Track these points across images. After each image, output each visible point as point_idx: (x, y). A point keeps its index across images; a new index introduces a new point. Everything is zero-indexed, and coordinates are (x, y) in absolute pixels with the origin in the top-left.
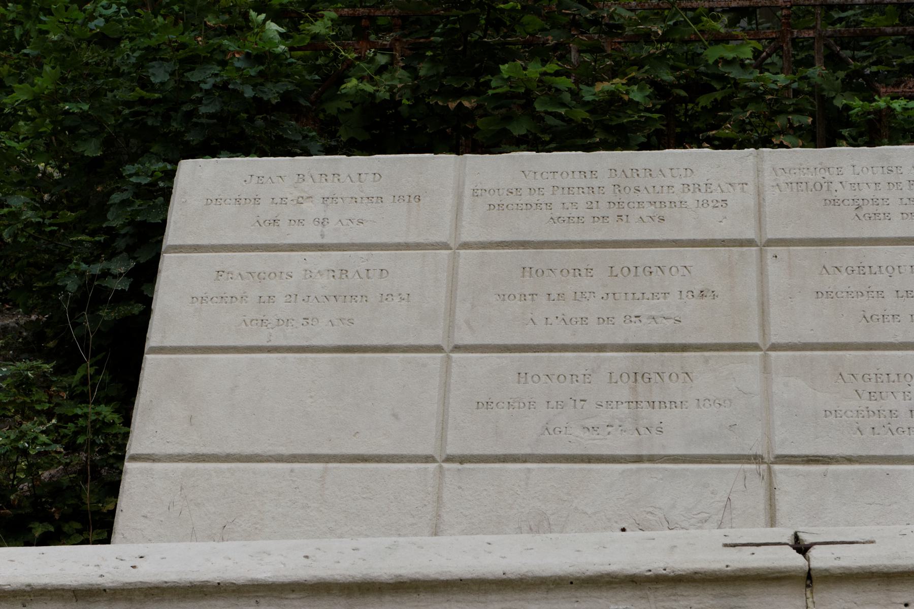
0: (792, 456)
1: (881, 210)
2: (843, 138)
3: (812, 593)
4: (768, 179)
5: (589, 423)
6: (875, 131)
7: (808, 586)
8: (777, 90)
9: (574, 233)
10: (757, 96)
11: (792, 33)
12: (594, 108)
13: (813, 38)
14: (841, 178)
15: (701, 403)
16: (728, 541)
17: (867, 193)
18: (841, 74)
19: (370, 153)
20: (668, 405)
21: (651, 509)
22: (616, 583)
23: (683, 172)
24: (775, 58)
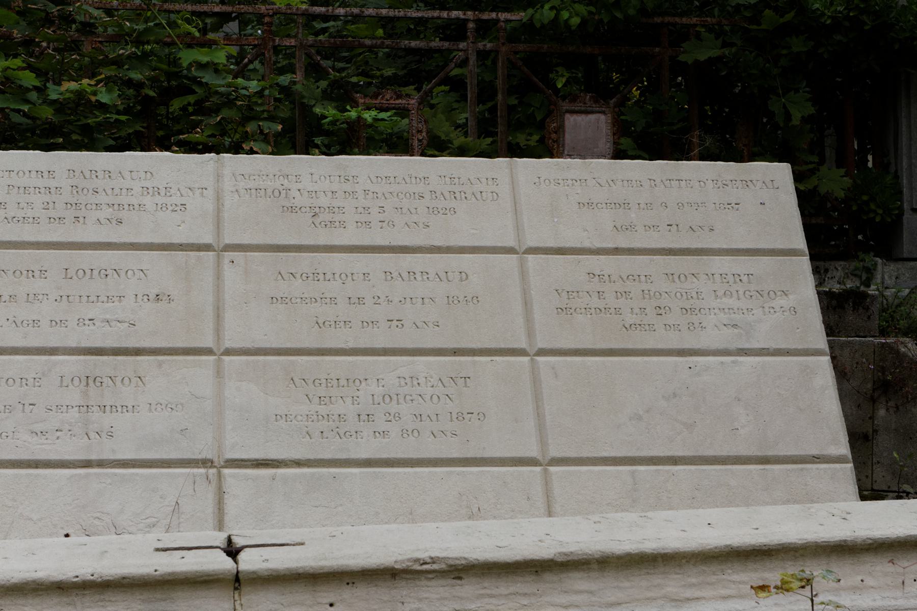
0: (242, 460)
1: (337, 218)
2: (317, 146)
3: (240, 595)
4: (228, 184)
5: (38, 427)
6: (348, 140)
7: (236, 589)
8: (249, 96)
9: (28, 234)
10: (229, 102)
11: (274, 41)
12: (59, 106)
13: (295, 47)
14: (300, 186)
15: (153, 407)
16: (160, 545)
17: (324, 201)
18: (323, 84)
19: (540, 157)
20: (119, 409)
21: (98, 515)
22: (42, 590)
23: (143, 175)
24: (256, 64)
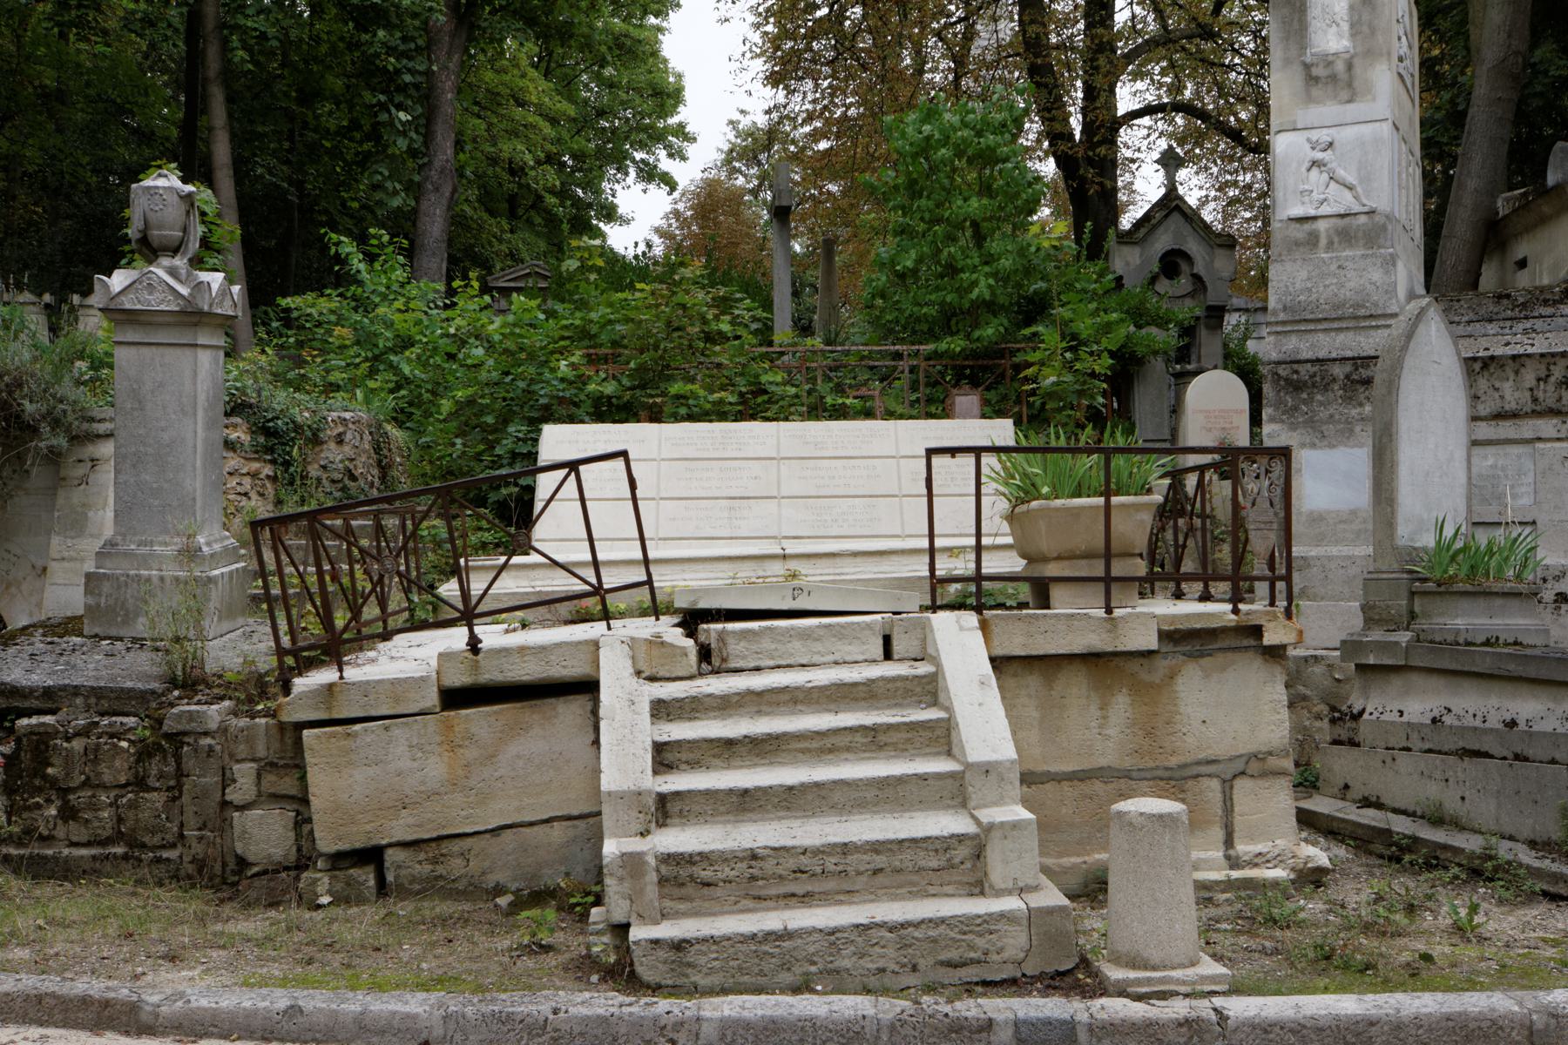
12: (714, 403)
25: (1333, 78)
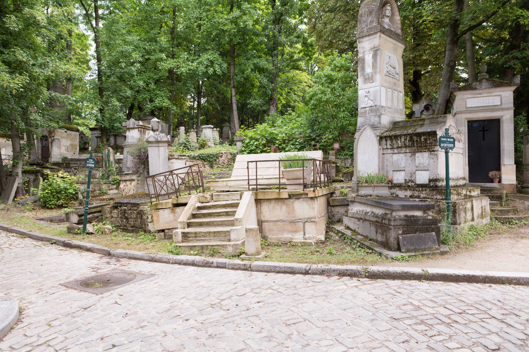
25: (369, 78)
